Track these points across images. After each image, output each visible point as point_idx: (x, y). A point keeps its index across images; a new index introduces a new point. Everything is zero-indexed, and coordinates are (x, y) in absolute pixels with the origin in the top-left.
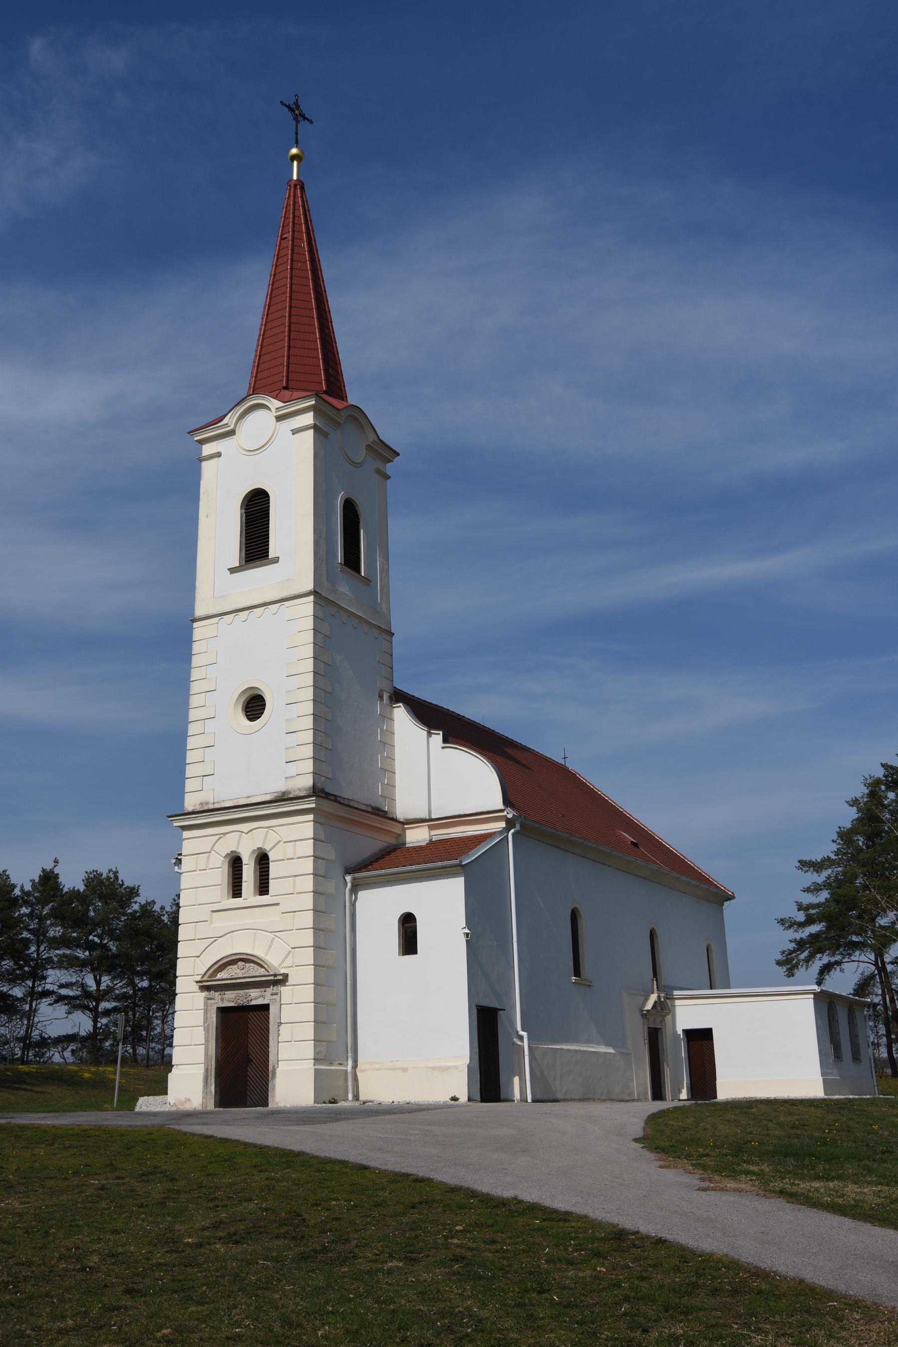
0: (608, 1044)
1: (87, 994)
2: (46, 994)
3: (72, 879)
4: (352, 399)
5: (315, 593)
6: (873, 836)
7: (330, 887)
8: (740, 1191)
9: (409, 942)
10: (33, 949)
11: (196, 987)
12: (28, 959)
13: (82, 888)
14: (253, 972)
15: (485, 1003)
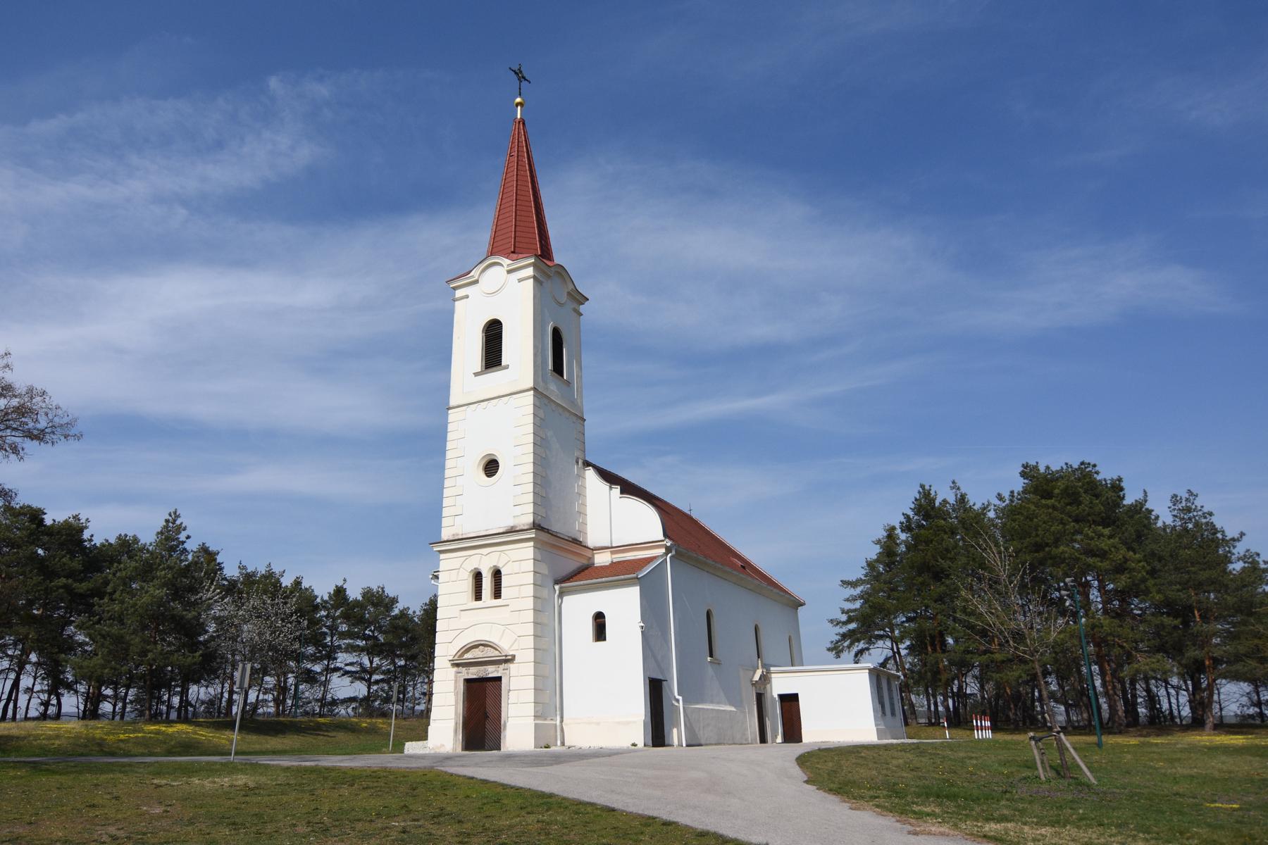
0: (731, 704)
1: (364, 670)
2: (337, 669)
3: (354, 593)
4: (557, 261)
5: (535, 389)
6: (889, 566)
7: (545, 593)
8: (942, 834)
9: (600, 631)
10: (329, 639)
11: (449, 664)
12: (325, 646)
13: (360, 598)
14: (489, 653)
15: (655, 676)
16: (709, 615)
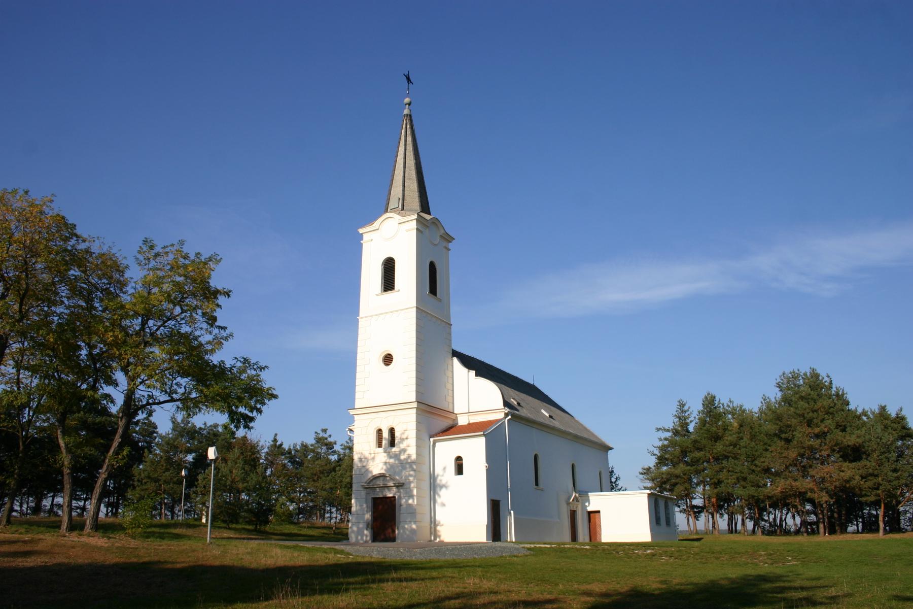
16: (573, 466)
